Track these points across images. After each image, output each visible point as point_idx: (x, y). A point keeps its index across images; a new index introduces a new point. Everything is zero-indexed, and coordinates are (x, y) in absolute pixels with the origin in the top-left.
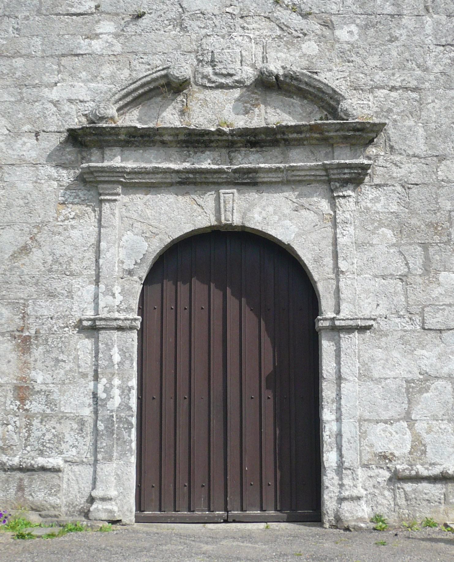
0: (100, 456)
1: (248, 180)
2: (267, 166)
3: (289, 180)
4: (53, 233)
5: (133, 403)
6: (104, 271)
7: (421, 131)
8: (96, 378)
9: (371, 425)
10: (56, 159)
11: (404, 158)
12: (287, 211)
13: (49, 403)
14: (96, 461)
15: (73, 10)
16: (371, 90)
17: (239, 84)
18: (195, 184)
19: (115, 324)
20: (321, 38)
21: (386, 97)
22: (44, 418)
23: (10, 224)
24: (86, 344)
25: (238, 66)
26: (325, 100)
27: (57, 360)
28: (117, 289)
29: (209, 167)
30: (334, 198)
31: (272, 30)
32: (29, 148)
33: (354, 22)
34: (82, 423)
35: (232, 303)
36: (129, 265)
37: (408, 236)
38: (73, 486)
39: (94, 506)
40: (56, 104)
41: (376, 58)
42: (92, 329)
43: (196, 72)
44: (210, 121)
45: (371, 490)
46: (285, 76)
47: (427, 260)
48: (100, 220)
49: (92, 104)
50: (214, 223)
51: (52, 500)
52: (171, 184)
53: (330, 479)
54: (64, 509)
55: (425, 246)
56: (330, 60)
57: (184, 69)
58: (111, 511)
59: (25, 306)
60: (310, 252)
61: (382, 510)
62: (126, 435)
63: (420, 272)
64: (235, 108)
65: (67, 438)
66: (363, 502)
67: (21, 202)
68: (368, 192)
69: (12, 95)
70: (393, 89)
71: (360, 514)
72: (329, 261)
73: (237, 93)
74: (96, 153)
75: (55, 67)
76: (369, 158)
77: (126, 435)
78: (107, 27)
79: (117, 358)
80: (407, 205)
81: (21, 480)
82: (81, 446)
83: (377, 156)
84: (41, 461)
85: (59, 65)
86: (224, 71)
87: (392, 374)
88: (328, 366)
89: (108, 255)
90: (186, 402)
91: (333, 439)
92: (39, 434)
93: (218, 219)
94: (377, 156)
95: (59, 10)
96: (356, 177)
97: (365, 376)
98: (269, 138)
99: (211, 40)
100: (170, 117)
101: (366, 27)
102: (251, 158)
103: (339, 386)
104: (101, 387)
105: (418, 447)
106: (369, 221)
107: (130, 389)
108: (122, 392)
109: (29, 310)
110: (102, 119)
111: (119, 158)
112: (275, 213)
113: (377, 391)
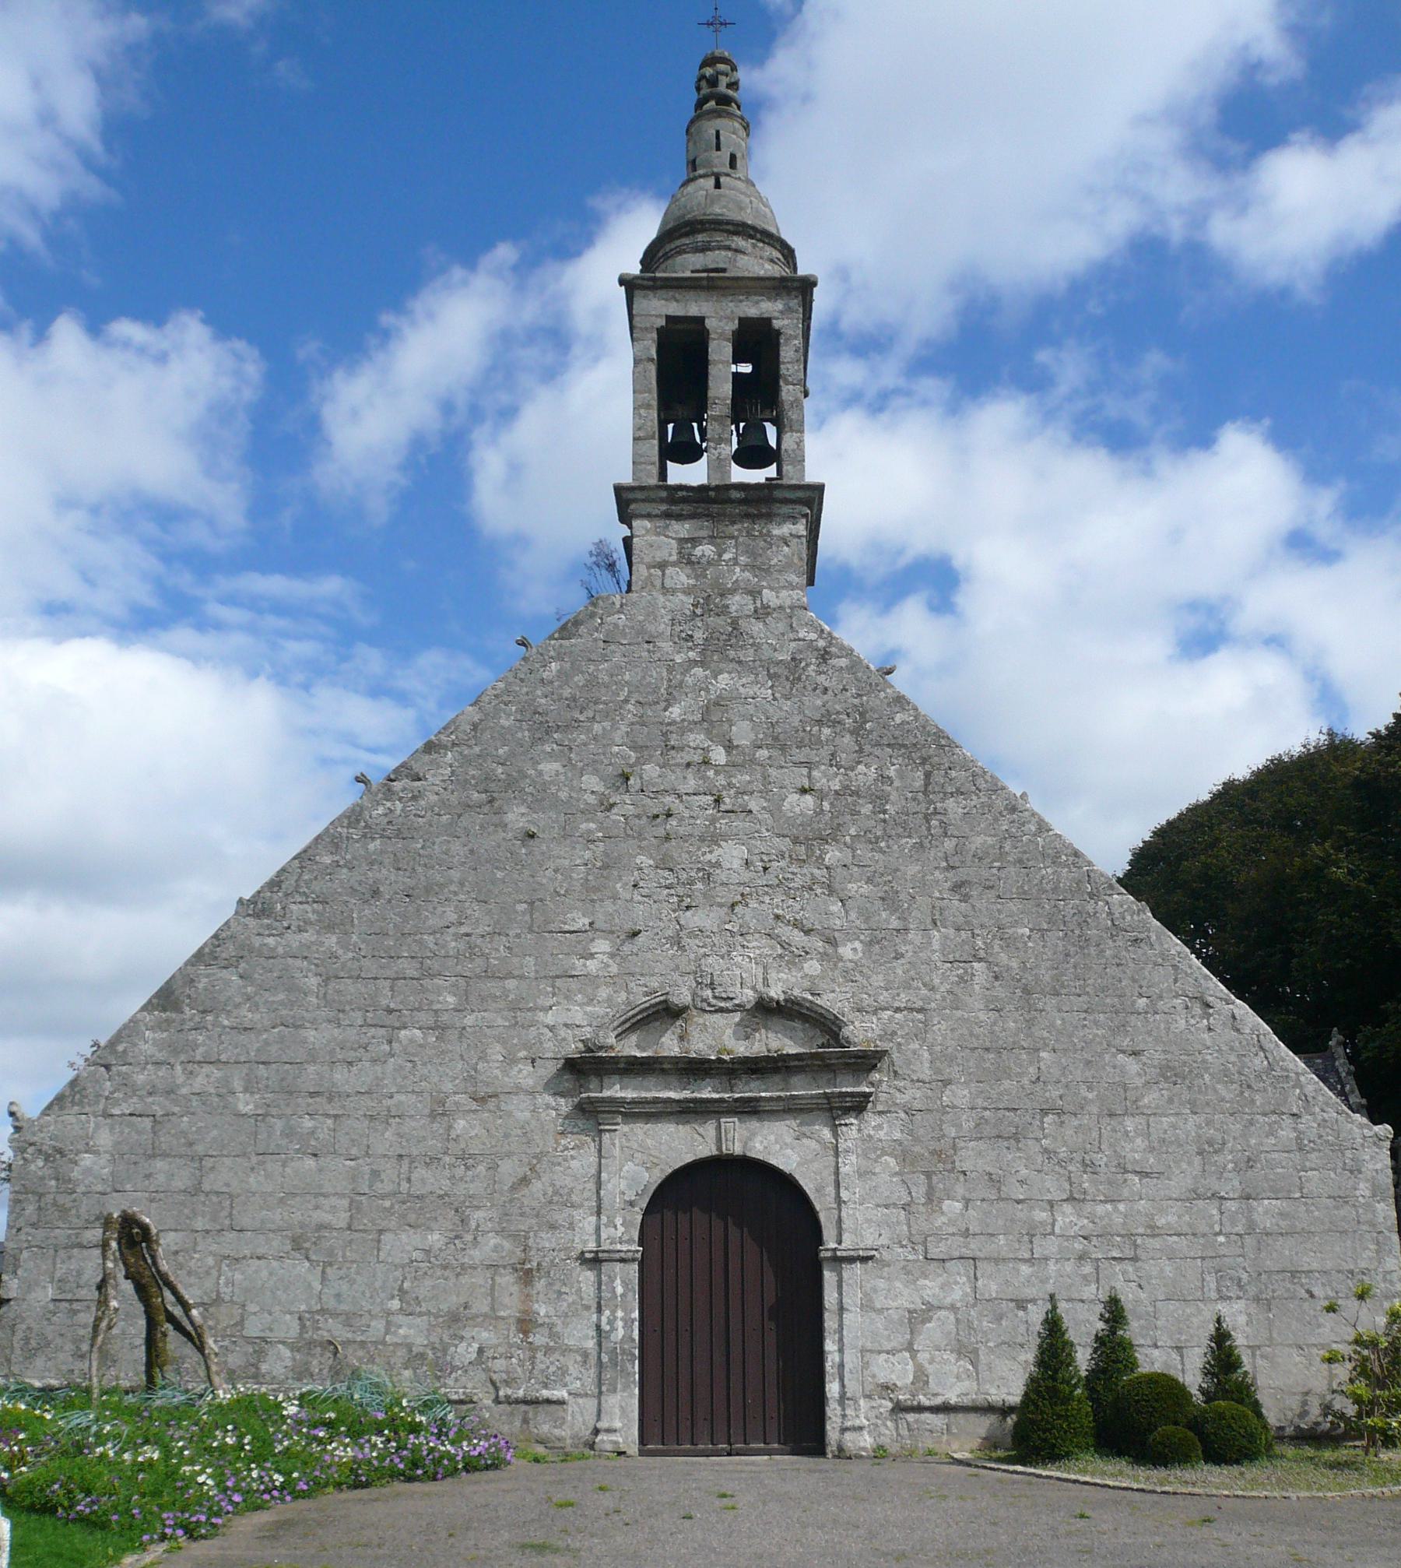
0: (604, 1388)
1: (749, 1109)
2: (768, 1094)
3: (791, 1108)
4: (553, 1164)
5: (636, 1335)
6: (605, 1204)
7: (926, 1055)
8: (599, 1310)
9: (874, 1356)
10: (553, 1087)
11: (908, 1083)
12: (789, 1140)
13: (553, 1335)
14: (600, 1393)
15: (567, 928)
16: (875, 1013)
17: (740, 1007)
18: (696, 1113)
19: (617, 1256)
20: (824, 957)
21: (891, 1019)
22: (548, 1350)
23: (509, 1154)
24: (588, 1276)
25: (738, 989)
26: (827, 1026)
27: (560, 1293)
28: (619, 1221)
29: (708, 1096)
30: (836, 1126)
31: (772, 948)
32: (525, 1075)
33: (858, 938)
34: (585, 1355)
35: (734, 1233)
36: (630, 1196)
37: (912, 1164)
38: (578, 1418)
39: (599, 1437)
40: (551, 1028)
41: (881, 977)
42: (594, 1261)
43: (694, 995)
44: (710, 1047)
45: (874, 1421)
46: (786, 1000)
47: (931, 1189)
48: (600, 1151)
49: (588, 1029)
50: (715, 1152)
51: (557, 1432)
52: (671, 1113)
53: (833, 1410)
54: (569, 1441)
55: (928, 1175)
56: (833, 980)
57: (682, 996)
58: (616, 1443)
59: (527, 1238)
61: (885, 1441)
62: (629, 1366)
63: (923, 1200)
64: (734, 1033)
65: (571, 1370)
66: (865, 1432)
67: (519, 1132)
68: (871, 1119)
69: (506, 1019)
70: (898, 1010)
71: (862, 1444)
72: (830, 1190)
73: (737, 1017)
74: (594, 1083)
75: (549, 989)
76: (872, 1084)
77: (629, 1366)
78: (602, 946)
79: (620, 1290)
80: (911, 1133)
81: (526, 1412)
82: (585, 1378)
83: (881, 1081)
84: (546, 1393)
85: (553, 987)
86: (724, 995)
87: (895, 1304)
88: (830, 1297)
89: (610, 1186)
90: (688, 1334)
91: (835, 1370)
92: (543, 1366)
93: (719, 1148)
94: (881, 1081)
95: (552, 927)
96: (859, 1105)
97: (867, 1306)
99: (710, 960)
100: (669, 1045)
101: (871, 943)
102: (752, 1085)
103: (841, 1316)
104: (604, 1319)
105: (921, 1378)
106: (871, 1149)
107: (633, 1321)
108: (624, 1324)
109: (531, 1242)
110: (601, 1048)
111: (618, 1087)
112: (777, 1142)
113: (880, 1323)
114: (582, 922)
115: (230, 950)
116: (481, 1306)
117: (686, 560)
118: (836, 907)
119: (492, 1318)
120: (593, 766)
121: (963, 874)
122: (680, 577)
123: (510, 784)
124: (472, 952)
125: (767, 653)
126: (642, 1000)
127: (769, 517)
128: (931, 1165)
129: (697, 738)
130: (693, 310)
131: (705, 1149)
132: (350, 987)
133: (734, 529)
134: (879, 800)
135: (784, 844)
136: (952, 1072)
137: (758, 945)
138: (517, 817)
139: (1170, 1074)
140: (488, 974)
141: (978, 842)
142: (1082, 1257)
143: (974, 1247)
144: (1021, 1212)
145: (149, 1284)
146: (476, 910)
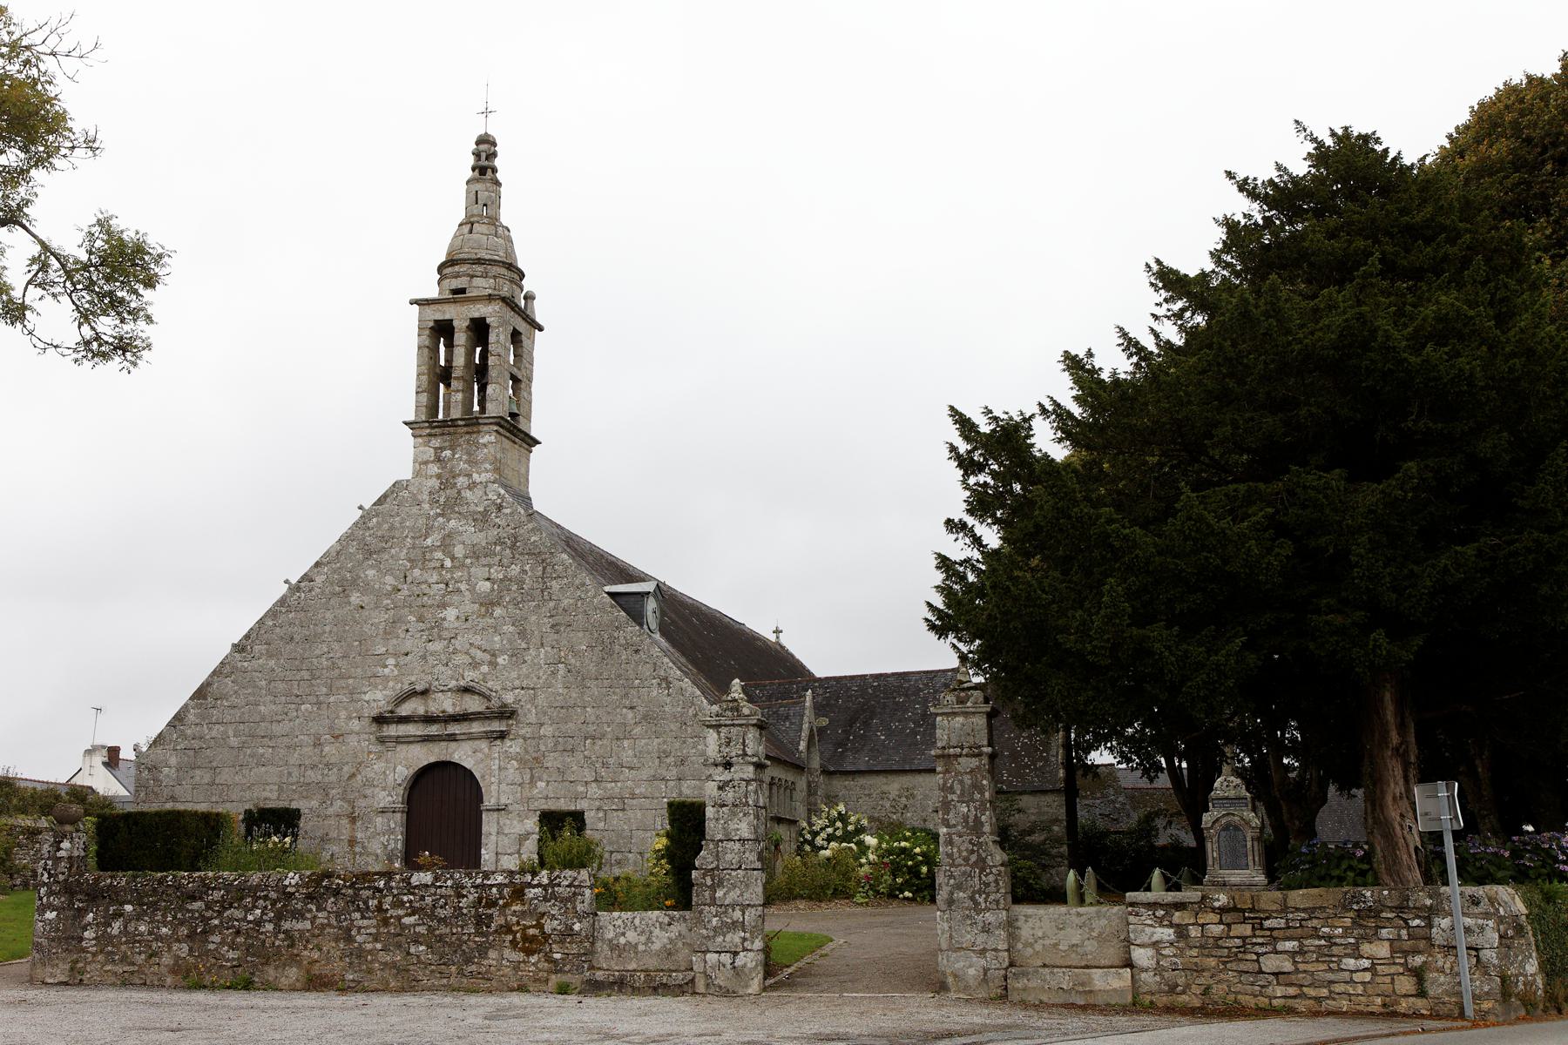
1: (452, 738)
3: (471, 737)
20: (490, 663)
22: (361, 854)
47: (532, 776)
60: (468, 763)
68: (508, 743)
96: (502, 736)
115: (227, 669)
117: (438, 460)
120: (389, 571)
121: (558, 619)
122: (434, 469)
124: (334, 666)
125: (472, 508)
134: (521, 583)
136: (546, 719)
138: (355, 598)
140: (341, 677)
146: (336, 646)
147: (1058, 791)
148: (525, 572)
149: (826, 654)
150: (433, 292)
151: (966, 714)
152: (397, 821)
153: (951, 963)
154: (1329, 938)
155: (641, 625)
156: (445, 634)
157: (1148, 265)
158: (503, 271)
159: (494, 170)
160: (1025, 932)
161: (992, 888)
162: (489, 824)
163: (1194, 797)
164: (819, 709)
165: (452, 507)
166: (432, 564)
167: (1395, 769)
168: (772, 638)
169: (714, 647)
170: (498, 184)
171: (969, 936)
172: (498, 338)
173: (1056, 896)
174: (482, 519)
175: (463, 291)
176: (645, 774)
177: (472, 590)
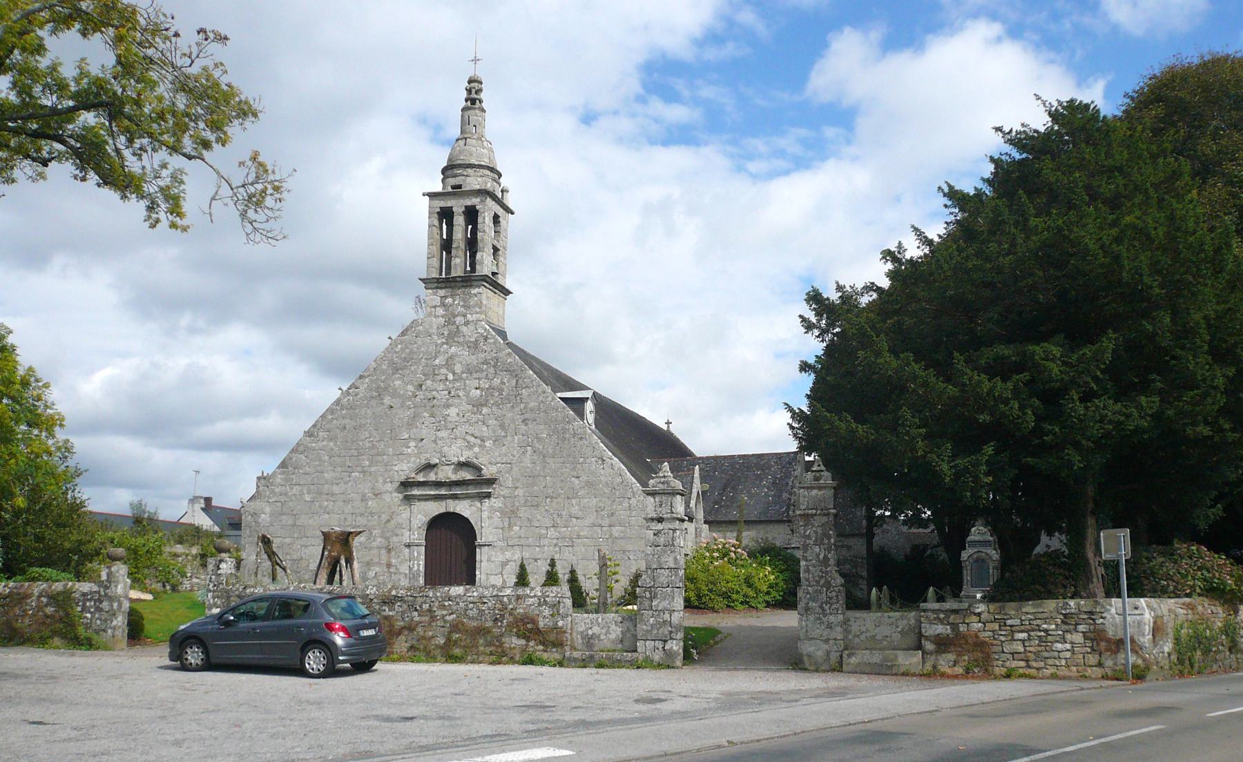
1: (455, 497)
3: (467, 497)
10: (398, 491)
24: (407, 550)
26: (477, 469)
32: (389, 487)
42: (408, 546)
60: (466, 514)
68: (493, 500)
78: (412, 444)
96: (488, 496)
98: (1125, 274)
100: (432, 477)
106: (492, 510)
114: (407, 436)
115: (301, 448)
116: (376, 560)
117: (443, 305)
118: (485, 429)
119: (379, 564)
120: (410, 382)
121: (527, 416)
122: (440, 311)
123: (386, 389)
124: (373, 447)
125: (467, 338)
126: (423, 462)
127: (471, 286)
128: (510, 514)
129: (444, 371)
130: (449, 205)
131: (442, 510)
132: (336, 459)
133: (459, 292)
134: (501, 391)
135: (470, 407)
136: (519, 485)
137: (460, 442)
138: (387, 400)
139: (589, 484)
140: (378, 454)
141: (532, 404)
142: (556, 545)
143: (523, 542)
144: (537, 530)
145: (271, 555)
146: (374, 433)
147: (859, 535)
148: (503, 383)
149: (704, 441)
150: (438, 188)
151: (820, 488)
152: (420, 553)
153: (807, 648)
154: (1046, 631)
155: (582, 419)
156: (450, 426)
157: (940, 188)
158: (488, 172)
159: (481, 101)
160: (854, 628)
161: (834, 600)
162: (481, 555)
163: (955, 539)
164: (703, 479)
165: (453, 337)
166: (439, 378)
167: (1091, 521)
168: (665, 427)
169: (643, 444)
170: (483, 111)
171: (819, 631)
172: (486, 220)
173: (864, 605)
174: (474, 346)
175: (460, 187)
176: (588, 521)
177: (467, 396)
